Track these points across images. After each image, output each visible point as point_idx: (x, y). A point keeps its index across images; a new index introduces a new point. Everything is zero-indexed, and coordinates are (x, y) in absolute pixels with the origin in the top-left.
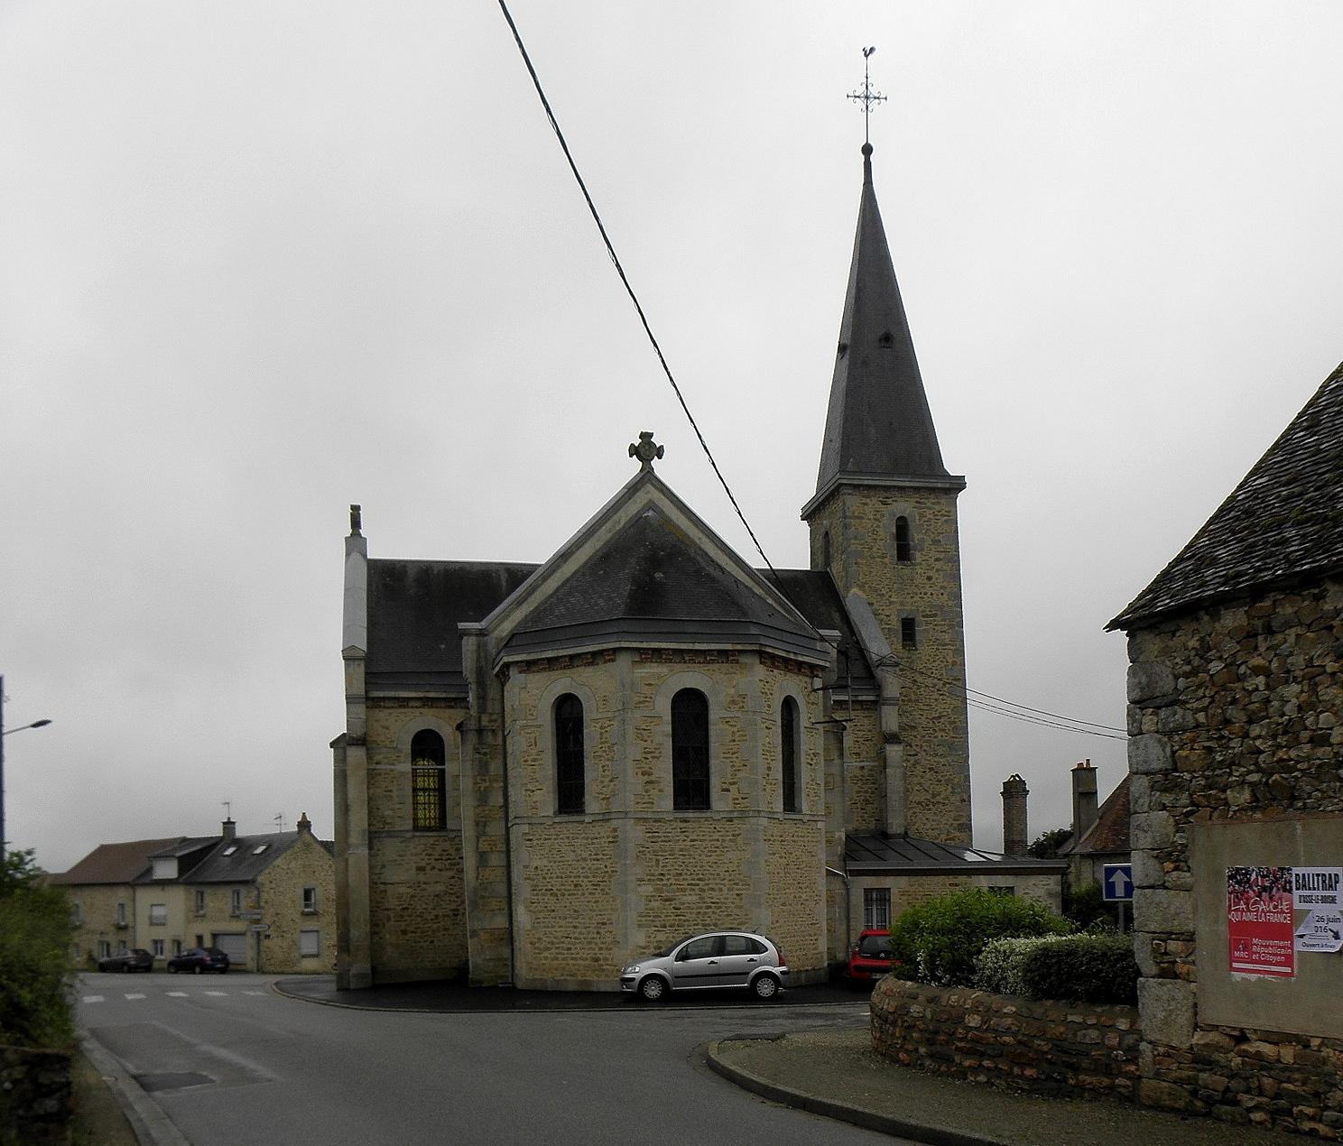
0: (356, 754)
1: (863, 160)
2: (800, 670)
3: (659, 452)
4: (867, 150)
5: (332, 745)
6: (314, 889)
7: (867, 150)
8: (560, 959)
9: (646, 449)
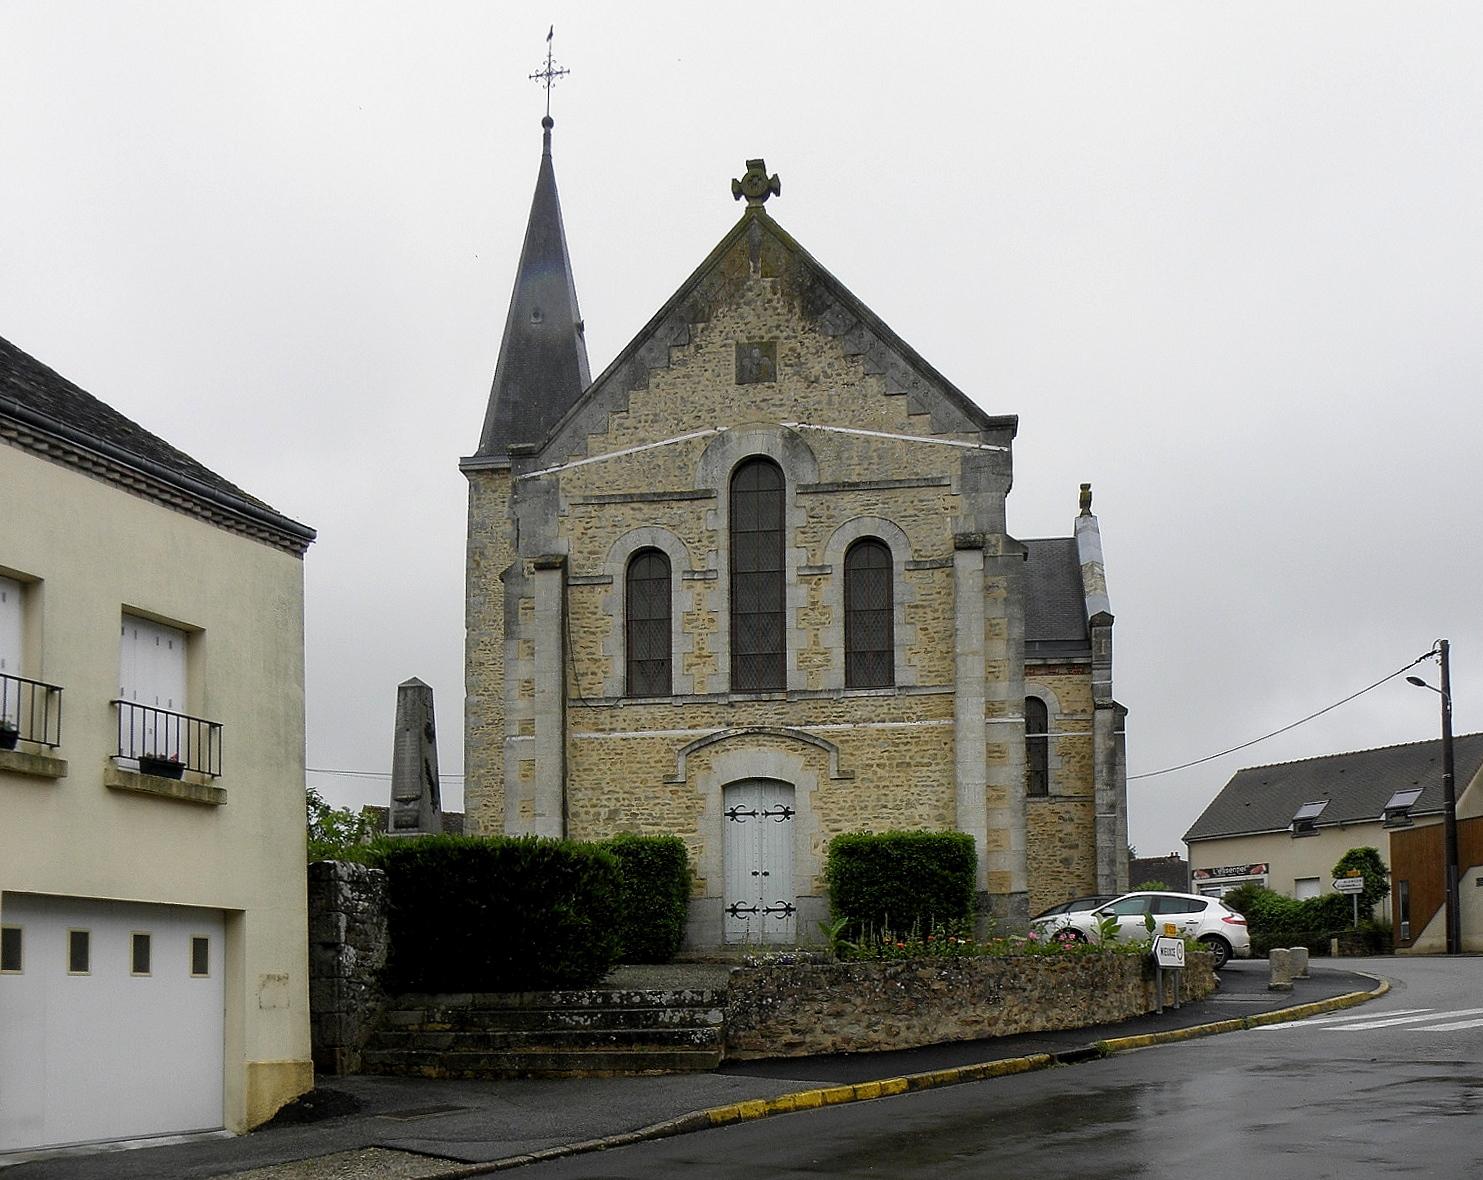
1: (543, 132)
3: (774, 187)
4: (548, 123)
7: (548, 123)
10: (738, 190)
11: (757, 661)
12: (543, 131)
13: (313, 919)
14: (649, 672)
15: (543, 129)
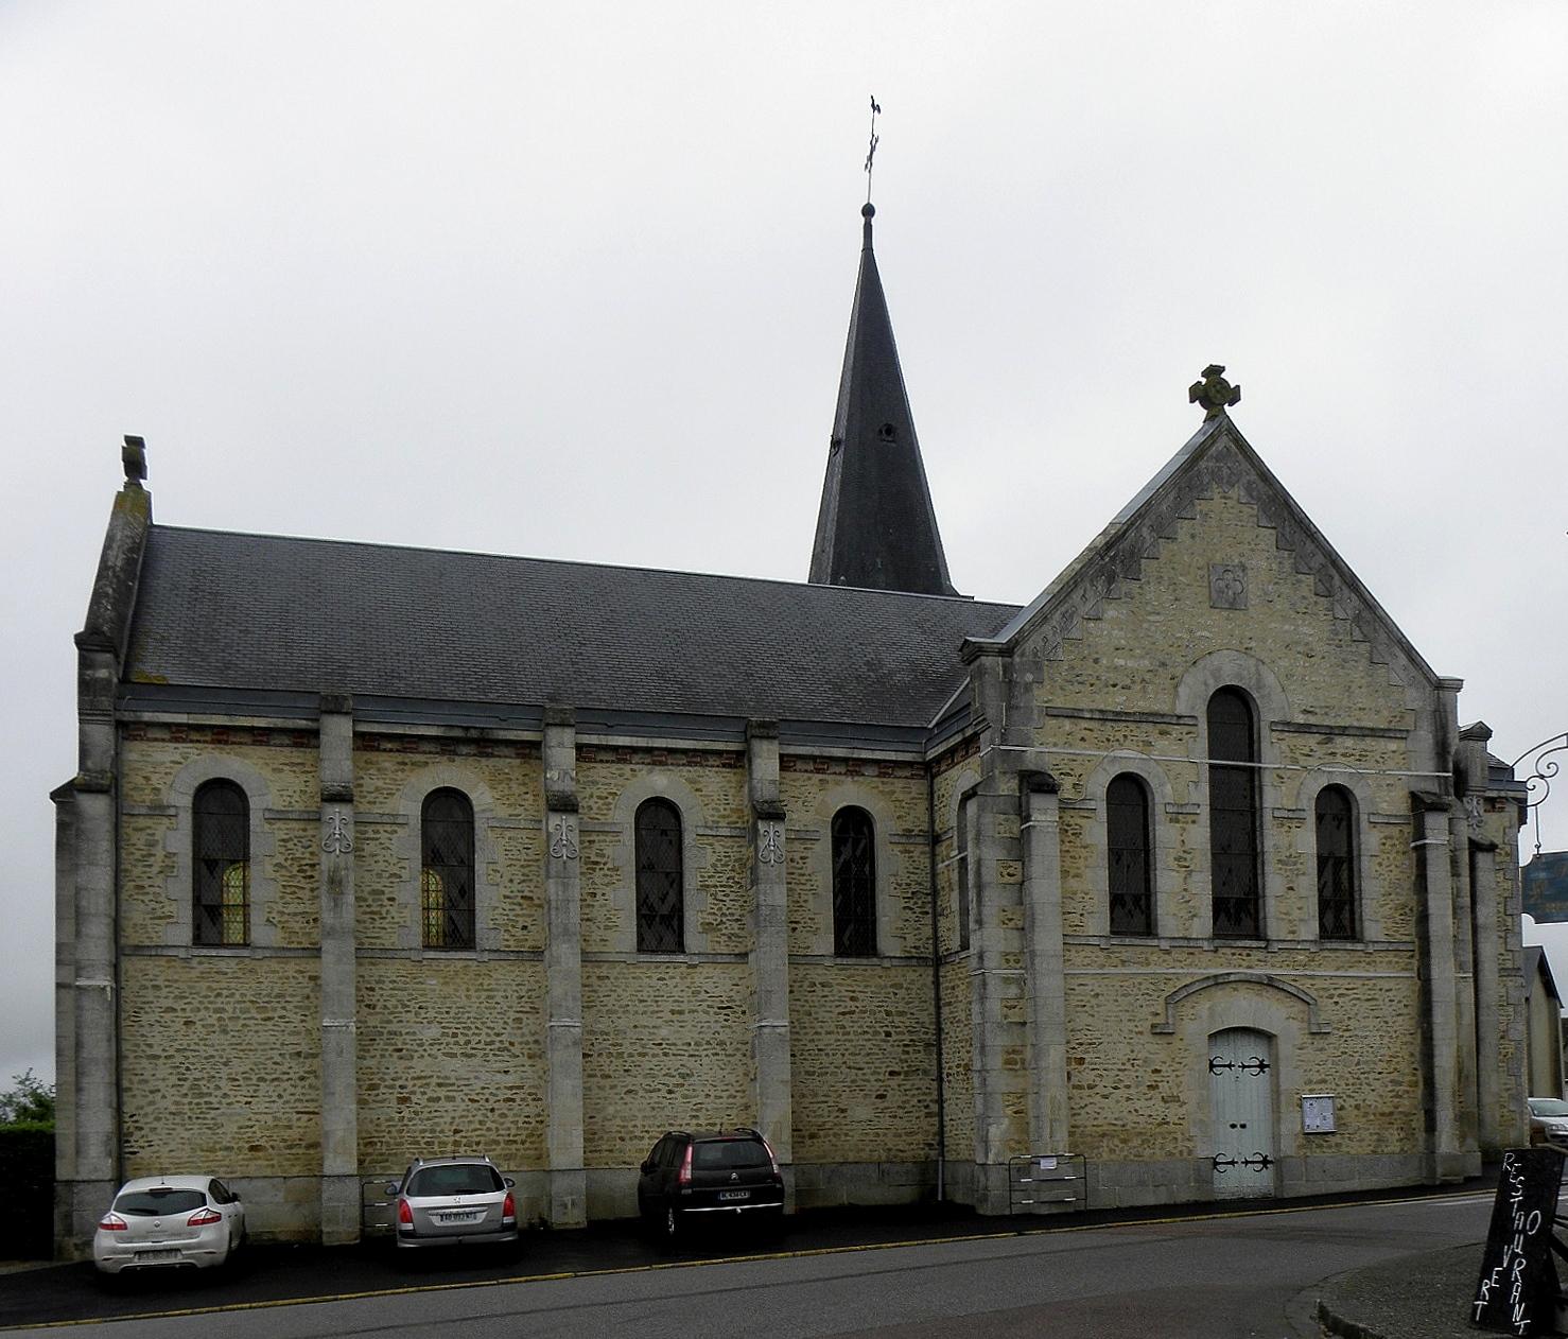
0: (95, 807)
1: (863, 223)
2: (1494, 807)
3: (1234, 396)
4: (868, 211)
5: (54, 796)
6: (427, 947)
7: (868, 211)
8: (477, 1123)
9: (1214, 392)
10: (1198, 394)
11: (1238, 911)
12: (862, 220)
13: (60, 872)
14: (1133, 909)
15: (863, 219)
